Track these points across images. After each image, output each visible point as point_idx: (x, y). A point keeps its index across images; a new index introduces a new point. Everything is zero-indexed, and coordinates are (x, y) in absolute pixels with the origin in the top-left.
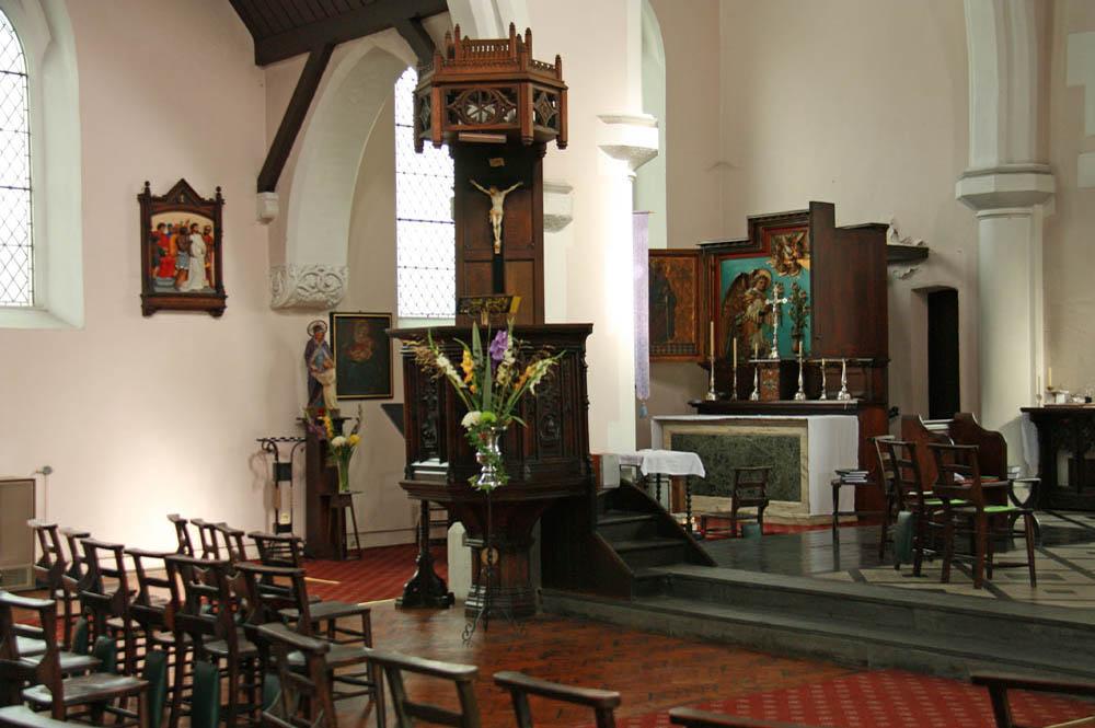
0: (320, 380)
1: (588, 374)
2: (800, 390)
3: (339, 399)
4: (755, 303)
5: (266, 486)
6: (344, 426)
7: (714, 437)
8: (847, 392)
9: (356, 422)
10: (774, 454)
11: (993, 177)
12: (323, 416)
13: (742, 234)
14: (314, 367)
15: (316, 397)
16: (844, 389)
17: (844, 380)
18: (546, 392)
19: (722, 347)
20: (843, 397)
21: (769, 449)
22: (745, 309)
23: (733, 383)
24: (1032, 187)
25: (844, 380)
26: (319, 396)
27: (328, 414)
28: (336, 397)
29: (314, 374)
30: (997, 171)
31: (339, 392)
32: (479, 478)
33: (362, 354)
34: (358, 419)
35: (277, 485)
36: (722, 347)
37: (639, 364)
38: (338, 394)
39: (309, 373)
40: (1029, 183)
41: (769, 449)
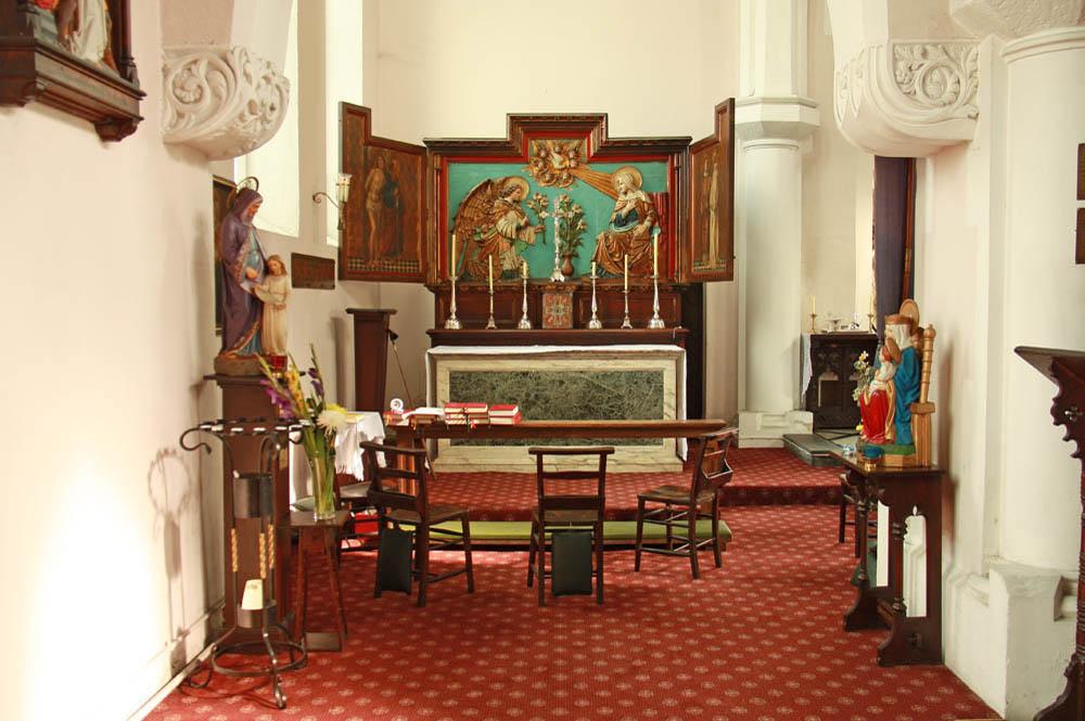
1: (873, 187)
2: (594, 316)
4: (509, 215)
5: (1054, 570)
7: (525, 374)
8: (660, 318)
10: (623, 392)
11: (760, 106)
13: (499, 131)
16: (656, 316)
17: (656, 307)
20: (656, 323)
21: (616, 387)
22: (495, 222)
23: (489, 309)
24: (795, 118)
25: (656, 307)
30: (765, 101)
37: (924, 173)
40: (792, 114)
41: (616, 387)
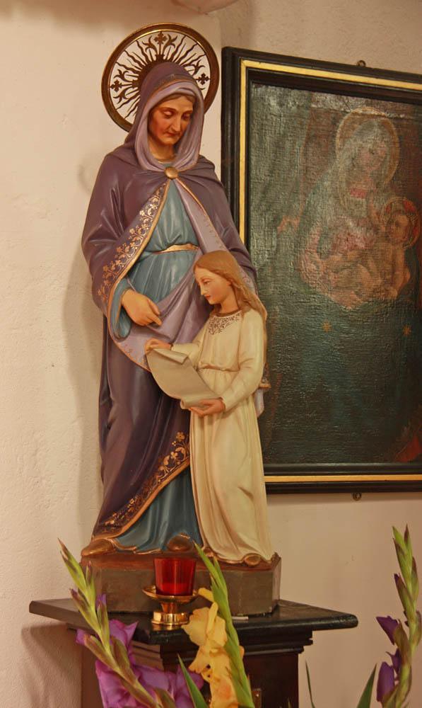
0: (168, 383)
3: (272, 489)
6: (306, 658)
9: (385, 649)
12: (191, 605)
14: (138, 305)
15: (139, 490)
18: (355, 143)
19: (215, 75)
26: (166, 479)
27: (217, 592)
28: (262, 480)
29: (136, 347)
31: (273, 458)
32: (318, 108)
33: (351, 224)
34: (387, 624)
35: (200, 376)
36: (215, 75)
38: (268, 471)
39: (109, 344)
